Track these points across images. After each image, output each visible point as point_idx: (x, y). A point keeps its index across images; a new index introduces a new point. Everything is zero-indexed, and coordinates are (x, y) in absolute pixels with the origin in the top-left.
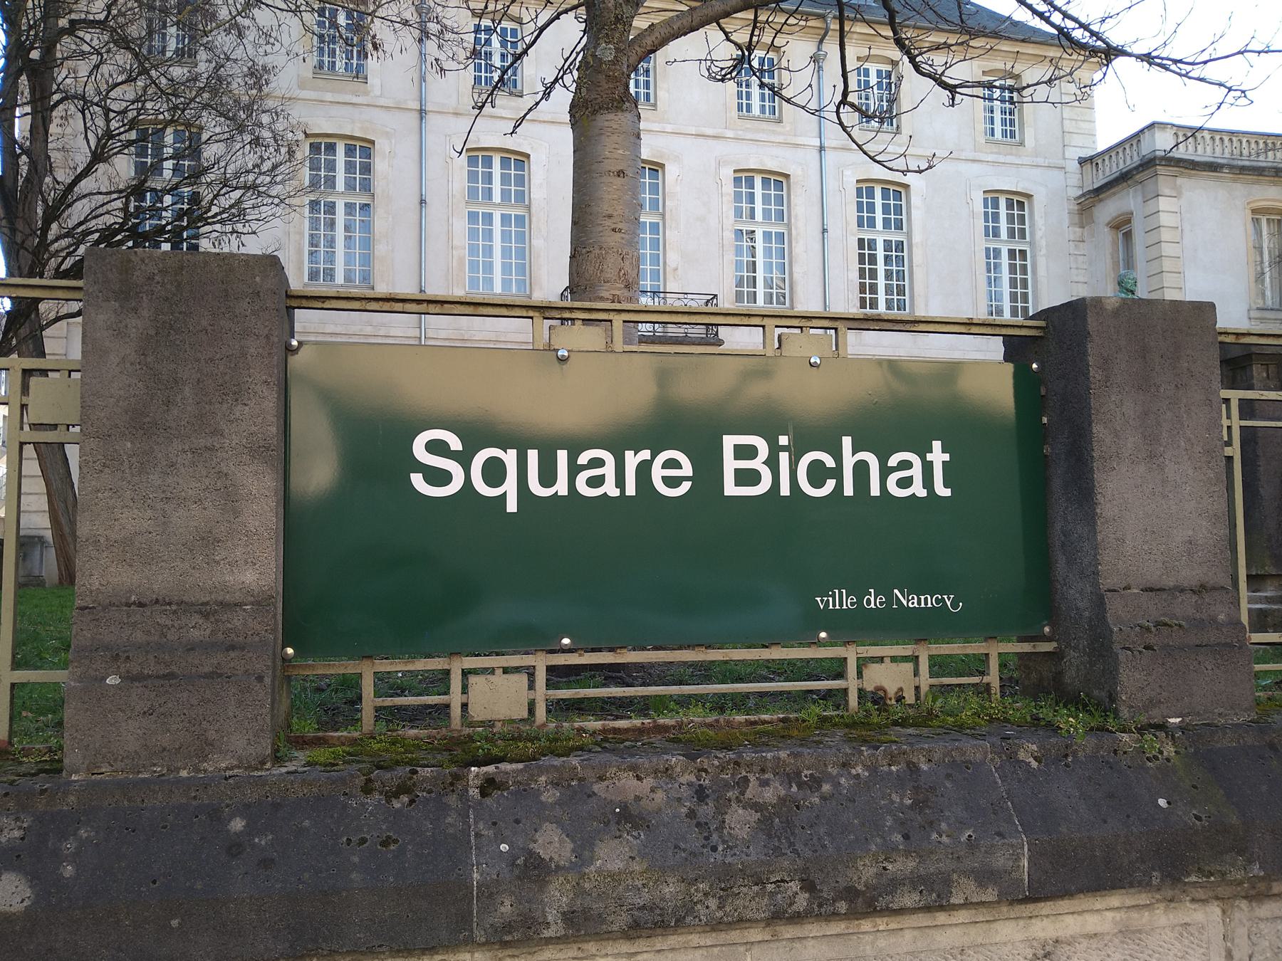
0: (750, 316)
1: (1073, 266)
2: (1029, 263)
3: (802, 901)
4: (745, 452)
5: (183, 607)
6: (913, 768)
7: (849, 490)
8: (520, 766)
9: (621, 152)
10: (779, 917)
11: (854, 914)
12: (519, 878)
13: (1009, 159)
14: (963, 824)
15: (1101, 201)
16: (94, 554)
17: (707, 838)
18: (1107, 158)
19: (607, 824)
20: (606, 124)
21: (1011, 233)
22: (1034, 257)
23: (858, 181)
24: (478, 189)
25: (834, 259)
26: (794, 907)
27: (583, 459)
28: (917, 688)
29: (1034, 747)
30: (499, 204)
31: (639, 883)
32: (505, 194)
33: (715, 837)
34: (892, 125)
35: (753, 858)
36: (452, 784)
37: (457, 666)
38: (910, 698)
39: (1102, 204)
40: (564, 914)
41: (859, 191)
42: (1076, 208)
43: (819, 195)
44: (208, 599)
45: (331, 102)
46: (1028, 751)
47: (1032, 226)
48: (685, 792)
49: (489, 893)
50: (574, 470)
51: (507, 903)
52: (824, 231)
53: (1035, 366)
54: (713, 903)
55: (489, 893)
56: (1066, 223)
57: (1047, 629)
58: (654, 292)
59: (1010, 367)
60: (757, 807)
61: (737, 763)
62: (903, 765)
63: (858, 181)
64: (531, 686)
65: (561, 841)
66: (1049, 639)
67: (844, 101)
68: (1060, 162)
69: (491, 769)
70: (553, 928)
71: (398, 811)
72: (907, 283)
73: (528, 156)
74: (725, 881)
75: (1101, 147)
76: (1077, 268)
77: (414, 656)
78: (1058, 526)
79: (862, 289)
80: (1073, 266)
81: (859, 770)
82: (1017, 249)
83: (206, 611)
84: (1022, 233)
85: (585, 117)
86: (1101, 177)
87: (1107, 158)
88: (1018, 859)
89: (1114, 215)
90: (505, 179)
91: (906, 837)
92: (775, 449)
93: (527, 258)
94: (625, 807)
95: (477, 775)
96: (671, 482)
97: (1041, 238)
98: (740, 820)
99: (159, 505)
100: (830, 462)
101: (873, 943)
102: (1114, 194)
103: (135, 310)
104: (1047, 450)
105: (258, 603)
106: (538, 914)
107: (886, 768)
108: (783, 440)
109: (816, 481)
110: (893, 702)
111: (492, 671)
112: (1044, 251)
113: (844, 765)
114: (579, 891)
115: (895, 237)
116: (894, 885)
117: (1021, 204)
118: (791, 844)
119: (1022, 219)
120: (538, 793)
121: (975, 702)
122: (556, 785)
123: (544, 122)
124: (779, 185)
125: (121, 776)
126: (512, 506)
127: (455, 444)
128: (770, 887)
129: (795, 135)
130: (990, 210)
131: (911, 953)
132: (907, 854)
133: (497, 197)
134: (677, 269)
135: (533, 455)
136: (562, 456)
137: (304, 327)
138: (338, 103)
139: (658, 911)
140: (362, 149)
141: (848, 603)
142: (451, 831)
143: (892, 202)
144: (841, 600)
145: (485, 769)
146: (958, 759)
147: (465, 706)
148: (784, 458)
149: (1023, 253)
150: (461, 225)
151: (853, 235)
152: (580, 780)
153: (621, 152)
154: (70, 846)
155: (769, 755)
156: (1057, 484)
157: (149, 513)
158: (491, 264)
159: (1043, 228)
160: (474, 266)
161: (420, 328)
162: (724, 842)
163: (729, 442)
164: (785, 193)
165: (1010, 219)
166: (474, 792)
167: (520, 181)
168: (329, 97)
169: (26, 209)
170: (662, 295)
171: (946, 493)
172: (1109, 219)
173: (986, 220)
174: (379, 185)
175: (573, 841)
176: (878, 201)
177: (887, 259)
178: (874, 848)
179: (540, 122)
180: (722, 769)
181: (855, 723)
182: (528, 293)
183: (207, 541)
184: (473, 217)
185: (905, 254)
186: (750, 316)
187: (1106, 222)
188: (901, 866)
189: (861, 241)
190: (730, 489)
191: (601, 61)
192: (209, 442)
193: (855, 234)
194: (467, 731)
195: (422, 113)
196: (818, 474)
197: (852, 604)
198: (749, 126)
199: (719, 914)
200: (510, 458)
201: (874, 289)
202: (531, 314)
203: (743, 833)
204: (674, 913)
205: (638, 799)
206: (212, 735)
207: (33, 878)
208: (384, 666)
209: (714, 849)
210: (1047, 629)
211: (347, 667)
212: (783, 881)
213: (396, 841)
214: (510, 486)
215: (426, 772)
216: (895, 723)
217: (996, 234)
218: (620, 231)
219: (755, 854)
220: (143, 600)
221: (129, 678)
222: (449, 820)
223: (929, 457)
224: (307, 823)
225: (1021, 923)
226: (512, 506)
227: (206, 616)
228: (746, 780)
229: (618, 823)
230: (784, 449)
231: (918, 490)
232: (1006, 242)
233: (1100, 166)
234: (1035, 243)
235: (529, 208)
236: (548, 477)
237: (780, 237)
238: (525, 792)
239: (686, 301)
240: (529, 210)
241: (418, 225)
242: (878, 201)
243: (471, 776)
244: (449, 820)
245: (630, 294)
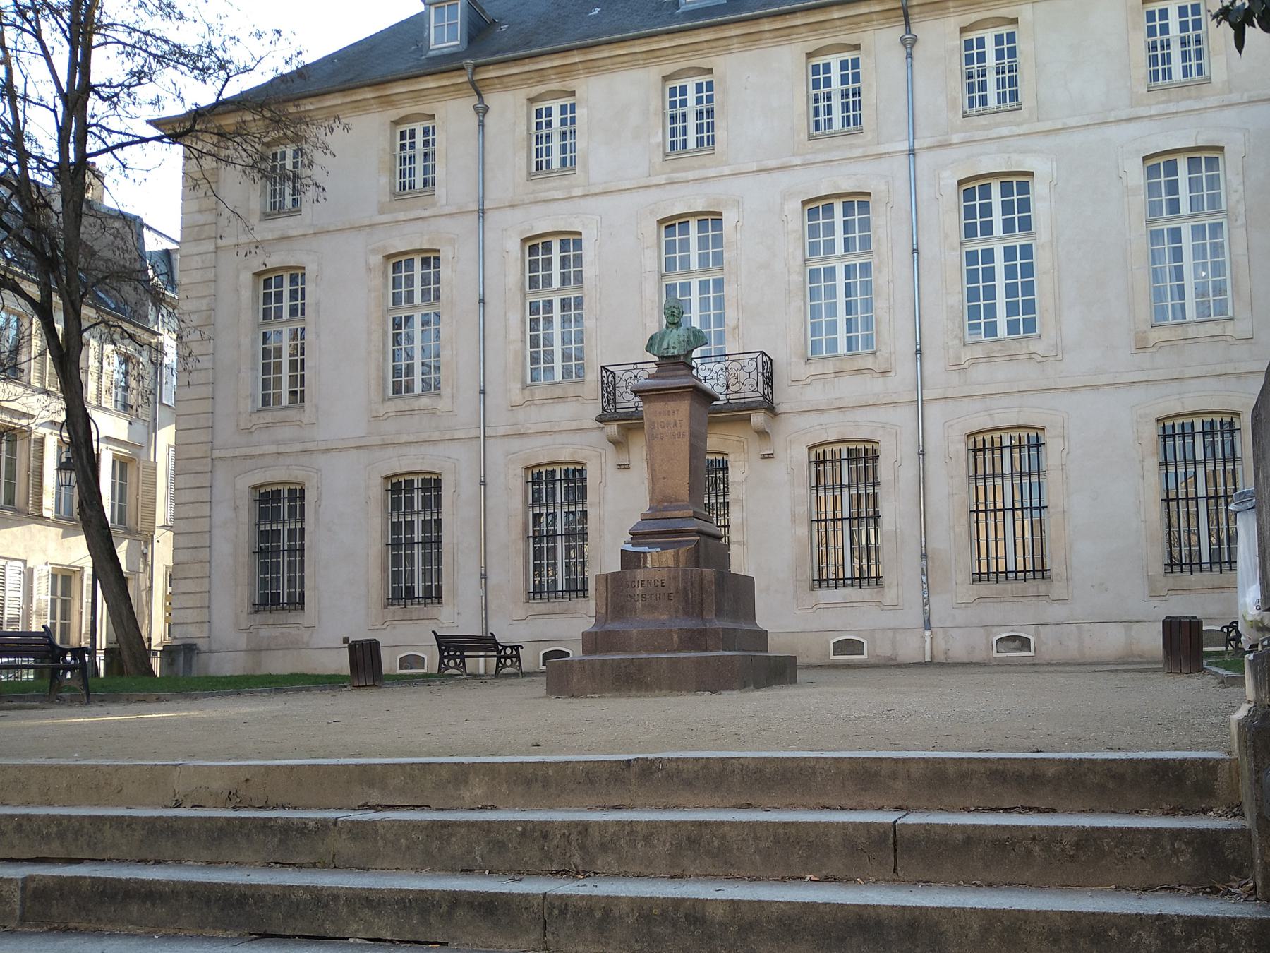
13: (1183, 106)
21: (1008, 227)
45: (404, 221)
90: (1194, 185)
97: (1238, 202)
115: (1018, 241)
123: (596, 194)
134: (737, 327)
137: (383, 440)
138: (410, 220)
140: (431, 259)
159: (1241, 188)
161: (922, 400)
168: (402, 216)
176: (996, 199)
179: (592, 195)
195: (482, 212)
198: (821, 146)
239: (636, 372)
242: (996, 199)
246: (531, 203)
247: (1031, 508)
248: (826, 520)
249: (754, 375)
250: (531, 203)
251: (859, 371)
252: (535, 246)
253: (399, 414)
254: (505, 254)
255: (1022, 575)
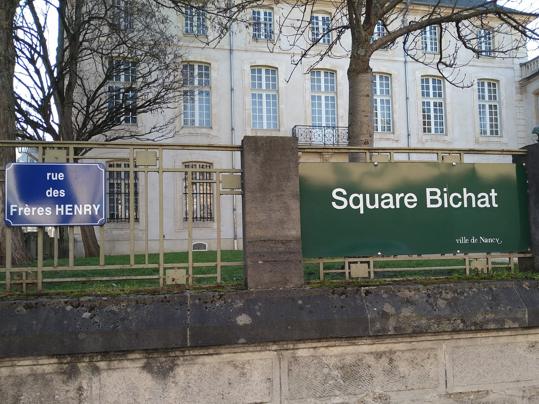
0: (433, 150)
1: (518, 111)
2: (498, 111)
3: (461, 326)
4: (433, 194)
5: (276, 241)
6: (491, 289)
7: (466, 205)
8: (376, 287)
9: (367, 88)
10: (456, 331)
11: (477, 331)
12: (381, 317)
13: (489, 65)
14: (508, 305)
15: (530, 82)
16: (251, 226)
17: (433, 308)
18: (532, 63)
19: (403, 303)
20: (362, 78)
21: (490, 98)
22: (500, 108)
23: (422, 76)
24: (256, 83)
25: (412, 112)
26: (459, 328)
27: (383, 197)
28: (488, 268)
29: (528, 283)
30: (265, 90)
31: (415, 320)
32: (267, 86)
33: (435, 307)
34: (436, 51)
35: (447, 313)
36: (357, 292)
37: (347, 260)
38: (485, 271)
39: (530, 84)
40: (394, 328)
41: (422, 80)
42: (519, 86)
43: (405, 82)
44: (283, 239)
46: (526, 285)
47: (499, 94)
48: (424, 295)
49: (373, 321)
50: (380, 200)
51: (378, 324)
52: (407, 98)
53: (524, 164)
54: (436, 326)
55: (373, 321)
56: (515, 93)
57: (529, 249)
58: (333, 127)
59: (515, 165)
60: (446, 299)
61: (438, 287)
62: (488, 288)
63: (422, 76)
64: (369, 267)
65: (391, 308)
66: (529, 253)
67: (440, 62)
68: (512, 66)
69: (367, 288)
70: (391, 332)
71: (343, 299)
72: (444, 121)
73: (277, 68)
74: (439, 319)
75: (530, 59)
76: (520, 113)
77: (333, 259)
78: (532, 216)
79: (424, 123)
80: (518, 111)
81: (475, 289)
82: (493, 104)
83: (283, 242)
84: (495, 97)
85: (354, 76)
86: (530, 72)
87: (532, 63)
88: (524, 315)
89: (536, 89)
90: (267, 79)
91: (491, 308)
92: (442, 192)
93: (278, 113)
94: (407, 299)
95: (364, 290)
96: (411, 203)
98: (441, 303)
99: (268, 212)
100: (460, 196)
101: (480, 341)
102: (536, 79)
103: (259, 154)
104: (528, 191)
105: (296, 240)
106: (387, 328)
107: (483, 289)
108: (445, 190)
109: (456, 202)
110: (480, 273)
111: (356, 262)
112: (505, 105)
113: (470, 288)
114: (398, 322)
115: (438, 100)
116: (488, 322)
117: (494, 85)
118: (457, 310)
119: (495, 91)
120: (381, 295)
121: (506, 273)
122: (386, 293)
124: (387, 78)
125: (264, 290)
126: (362, 212)
127: (345, 193)
128: (452, 322)
129: (394, 56)
130: (480, 88)
131: (492, 344)
132: (492, 313)
133: (264, 87)
135: (368, 196)
136: (377, 196)
139: (420, 328)
141: (466, 241)
142: (359, 304)
143: (437, 85)
144: (464, 240)
145: (366, 288)
146: (504, 287)
147: (349, 273)
148: (445, 195)
149: (495, 106)
150: (249, 100)
151: (420, 100)
152: (393, 291)
153: (367, 88)
154: (257, 307)
155: (448, 285)
156: (532, 203)
157: (266, 214)
158: (262, 116)
159: (504, 95)
160: (254, 117)
162: (438, 309)
163: (428, 190)
164: (389, 82)
165: (490, 91)
166: (363, 294)
167: (274, 79)
169: (69, 97)
170: (336, 128)
171: (496, 206)
172: (534, 90)
173: (479, 92)
174: (213, 83)
175: (394, 308)
176: (431, 85)
177: (435, 110)
178: (482, 311)
180: (434, 289)
181: (469, 279)
182: (278, 128)
183: (282, 222)
184: (254, 96)
185: (443, 108)
186: (433, 150)
187: (532, 92)
188: (490, 316)
189: (423, 103)
190: (429, 205)
191: (359, 55)
192: (281, 193)
193: (421, 99)
194: (351, 280)
195: (231, 51)
196: (456, 201)
197: (467, 242)
199: (438, 329)
200: (361, 197)
201: (429, 123)
202: (366, 151)
203: (443, 306)
204: (425, 329)
205: (411, 297)
206: (288, 278)
207: (250, 315)
208: (326, 261)
209: (435, 310)
210: (529, 249)
211: (315, 261)
212: (456, 320)
213: (345, 307)
214: (361, 206)
215: (349, 289)
216: (482, 279)
217: (483, 98)
218: (368, 116)
219: (447, 312)
220: (265, 240)
221: (265, 262)
222: (358, 302)
223: (491, 194)
224: (319, 302)
225: (525, 336)
226: (362, 212)
227: (283, 244)
228: (441, 292)
229: (406, 303)
230: (445, 192)
231: (487, 205)
232: (488, 101)
233: (529, 67)
234: (500, 102)
235: (278, 91)
236: (372, 203)
237: (388, 102)
238: (377, 295)
240: (278, 92)
241: (230, 100)
242: (431, 85)
243: (362, 290)
244: (358, 302)
245: (371, 139)
246: (255, 51)
247: (203, 194)
248: (200, 194)
249: (321, 135)
250: (255, 51)
251: (388, 139)
252: (255, 69)
253: (190, 134)
254: (243, 71)
255: (202, 218)
